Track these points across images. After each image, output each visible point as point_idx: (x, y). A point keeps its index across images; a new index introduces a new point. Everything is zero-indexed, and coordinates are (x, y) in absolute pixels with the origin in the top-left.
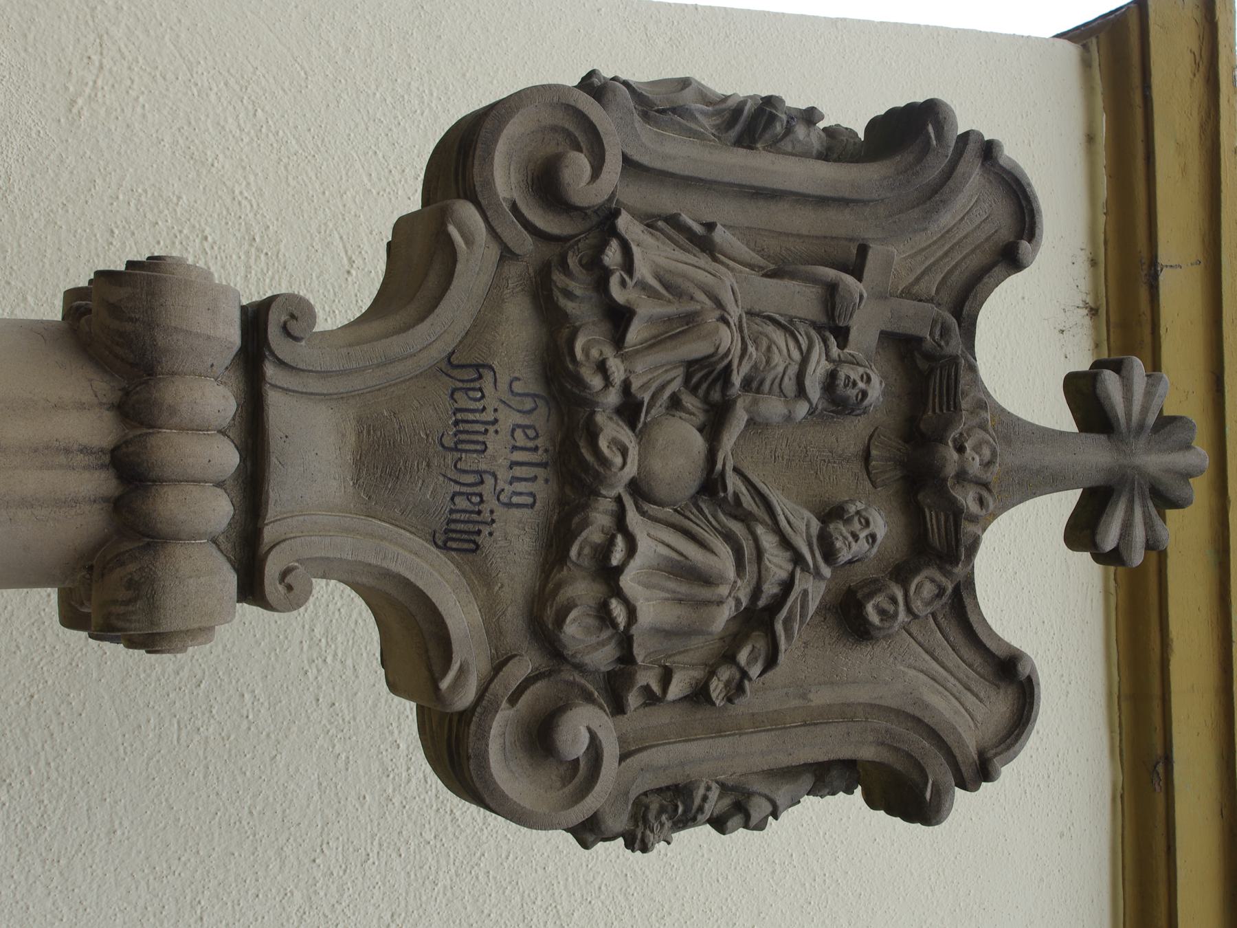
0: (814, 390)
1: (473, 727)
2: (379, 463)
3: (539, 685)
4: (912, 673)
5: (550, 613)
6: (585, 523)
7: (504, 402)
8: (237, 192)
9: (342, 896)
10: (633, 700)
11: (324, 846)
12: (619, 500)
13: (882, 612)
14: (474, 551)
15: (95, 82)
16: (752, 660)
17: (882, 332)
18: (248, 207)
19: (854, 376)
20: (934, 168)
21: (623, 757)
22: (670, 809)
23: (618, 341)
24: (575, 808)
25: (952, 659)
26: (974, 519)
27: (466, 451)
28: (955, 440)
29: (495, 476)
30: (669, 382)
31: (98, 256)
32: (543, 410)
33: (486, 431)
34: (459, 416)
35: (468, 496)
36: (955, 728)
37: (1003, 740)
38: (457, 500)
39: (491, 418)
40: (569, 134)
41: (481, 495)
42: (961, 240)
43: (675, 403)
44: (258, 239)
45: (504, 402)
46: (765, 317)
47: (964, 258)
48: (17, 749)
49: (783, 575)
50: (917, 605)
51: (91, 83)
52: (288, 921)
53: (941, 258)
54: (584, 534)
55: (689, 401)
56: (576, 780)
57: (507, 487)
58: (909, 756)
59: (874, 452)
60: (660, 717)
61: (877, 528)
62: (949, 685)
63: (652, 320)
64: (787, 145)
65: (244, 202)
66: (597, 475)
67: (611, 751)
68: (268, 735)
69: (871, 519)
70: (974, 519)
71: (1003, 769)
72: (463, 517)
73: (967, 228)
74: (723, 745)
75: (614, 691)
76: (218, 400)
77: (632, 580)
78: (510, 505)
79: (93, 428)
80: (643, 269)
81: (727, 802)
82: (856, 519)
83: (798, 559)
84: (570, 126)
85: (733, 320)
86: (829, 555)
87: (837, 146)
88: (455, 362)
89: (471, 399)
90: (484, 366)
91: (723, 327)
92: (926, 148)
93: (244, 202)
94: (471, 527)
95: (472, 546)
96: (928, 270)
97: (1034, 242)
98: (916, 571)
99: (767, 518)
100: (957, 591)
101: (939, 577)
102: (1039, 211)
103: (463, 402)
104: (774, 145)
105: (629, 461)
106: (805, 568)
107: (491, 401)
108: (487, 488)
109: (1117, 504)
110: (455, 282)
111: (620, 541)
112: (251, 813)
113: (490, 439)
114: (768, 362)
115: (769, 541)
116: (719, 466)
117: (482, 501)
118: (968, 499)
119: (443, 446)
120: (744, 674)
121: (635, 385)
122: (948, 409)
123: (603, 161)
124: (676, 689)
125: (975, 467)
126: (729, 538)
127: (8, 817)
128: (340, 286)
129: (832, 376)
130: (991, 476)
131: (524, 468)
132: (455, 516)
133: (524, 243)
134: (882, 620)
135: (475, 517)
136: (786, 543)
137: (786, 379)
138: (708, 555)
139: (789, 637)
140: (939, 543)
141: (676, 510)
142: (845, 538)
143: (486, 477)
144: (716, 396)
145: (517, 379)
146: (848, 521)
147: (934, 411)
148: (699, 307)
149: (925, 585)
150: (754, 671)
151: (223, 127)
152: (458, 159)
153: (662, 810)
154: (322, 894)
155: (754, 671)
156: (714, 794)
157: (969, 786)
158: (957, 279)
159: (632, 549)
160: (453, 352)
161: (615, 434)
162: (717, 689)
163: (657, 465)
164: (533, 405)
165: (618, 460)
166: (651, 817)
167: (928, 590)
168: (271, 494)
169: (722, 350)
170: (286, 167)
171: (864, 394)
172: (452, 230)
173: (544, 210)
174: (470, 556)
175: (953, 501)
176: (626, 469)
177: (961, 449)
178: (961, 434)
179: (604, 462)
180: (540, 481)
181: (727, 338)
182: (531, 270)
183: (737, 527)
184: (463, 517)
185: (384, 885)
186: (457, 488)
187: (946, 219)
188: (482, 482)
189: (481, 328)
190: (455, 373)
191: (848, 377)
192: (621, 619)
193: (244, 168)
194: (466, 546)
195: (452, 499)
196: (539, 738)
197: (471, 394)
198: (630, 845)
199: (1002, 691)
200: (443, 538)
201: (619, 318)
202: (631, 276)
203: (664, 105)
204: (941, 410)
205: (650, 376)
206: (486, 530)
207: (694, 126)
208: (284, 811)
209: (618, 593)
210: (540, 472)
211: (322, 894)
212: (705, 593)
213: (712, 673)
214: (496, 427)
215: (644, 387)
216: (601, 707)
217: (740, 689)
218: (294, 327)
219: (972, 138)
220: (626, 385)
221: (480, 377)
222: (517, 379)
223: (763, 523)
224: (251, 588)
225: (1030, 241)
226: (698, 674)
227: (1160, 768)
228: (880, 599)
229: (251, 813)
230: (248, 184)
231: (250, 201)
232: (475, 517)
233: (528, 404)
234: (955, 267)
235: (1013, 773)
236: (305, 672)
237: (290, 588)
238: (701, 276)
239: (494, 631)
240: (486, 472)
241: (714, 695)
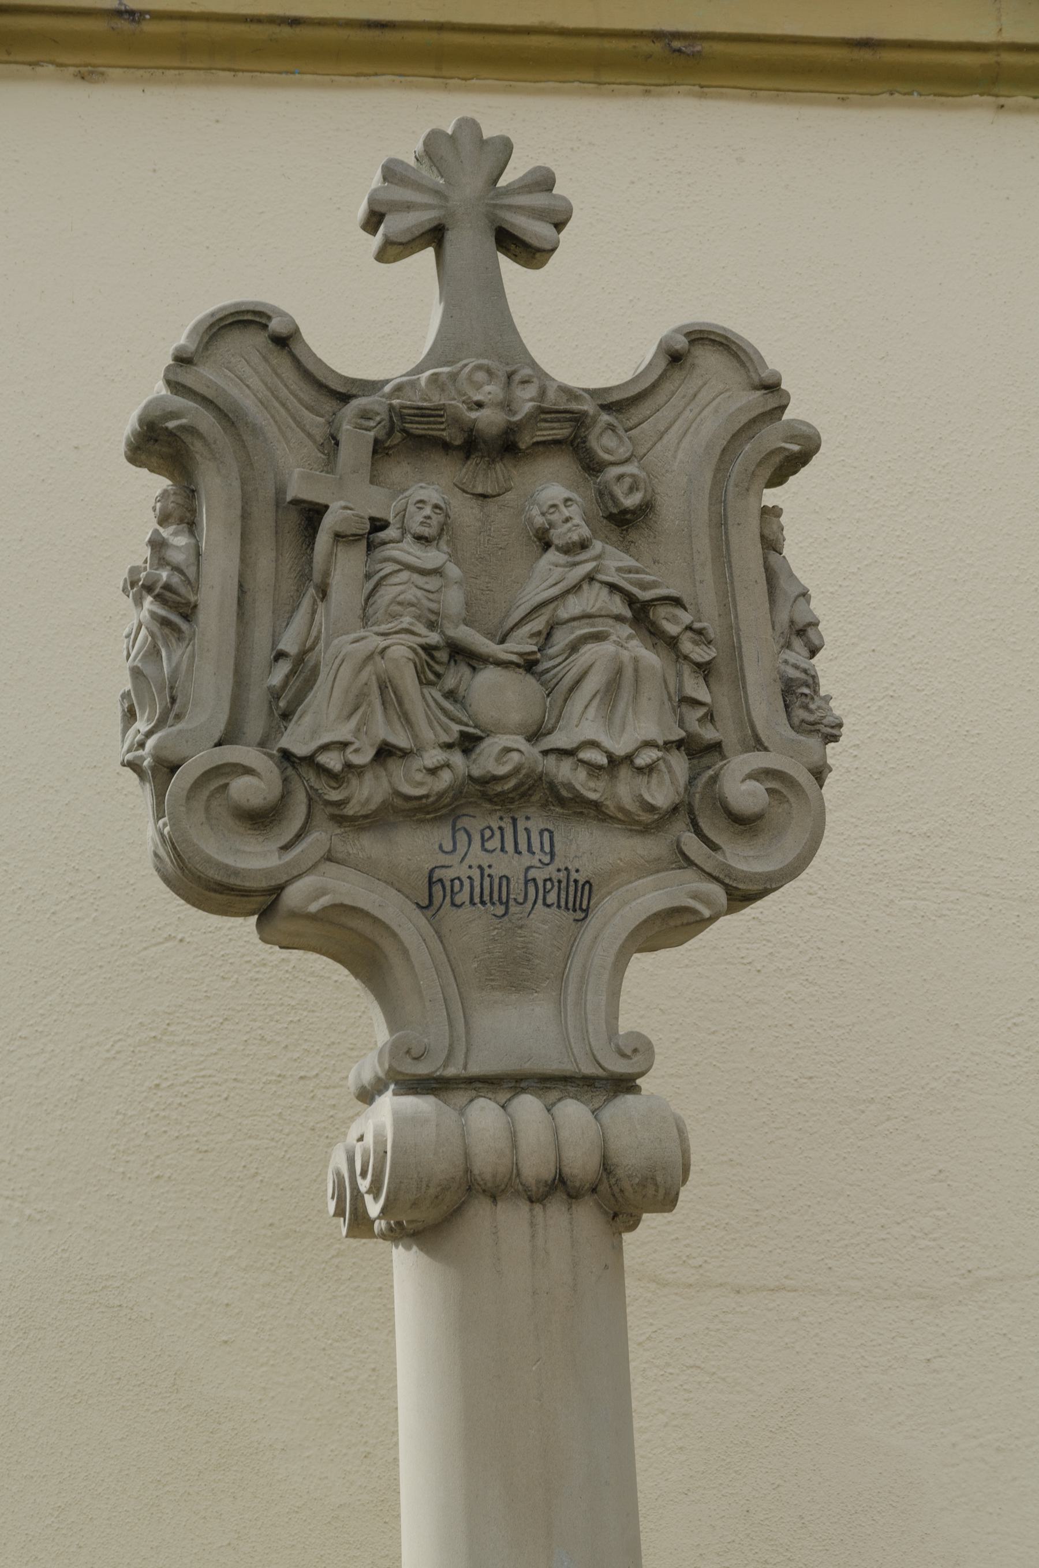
0: (432, 557)
1: (741, 886)
2: (514, 973)
3: (703, 823)
4: (680, 455)
5: (646, 817)
6: (569, 787)
7: (463, 859)
8: (108, 1055)
9: (791, 944)
10: (709, 734)
11: (745, 961)
12: (545, 753)
13: (632, 489)
14: (591, 885)
15: (7, 1198)
16: (674, 620)
17: (372, 482)
18: (120, 1043)
19: (419, 518)
20: (206, 421)
21: (759, 745)
22: (803, 699)
24: (808, 792)
25: (667, 413)
26: (543, 392)
27: (508, 894)
28: (470, 409)
29: (528, 869)
30: (435, 700)
31: (183, 1190)
33: (489, 876)
34: (477, 900)
35: (546, 893)
36: (731, 415)
37: (743, 364)
38: (549, 901)
39: (478, 871)
40: (212, 795)
41: (545, 881)
42: (269, 389)
43: (451, 695)
44: (153, 1034)
45: (463, 859)
46: (366, 604)
47: (286, 385)
48: (655, 1251)
49: (605, 591)
50: (623, 452)
51: (8, 1202)
52: (813, 996)
53: (288, 410)
54: (578, 787)
56: (783, 790)
57: (537, 857)
58: (759, 464)
59: (480, 490)
60: (725, 708)
61: (552, 490)
62: (691, 416)
63: (388, 721)
64: (191, 572)
65: (117, 1047)
66: (528, 776)
67: (758, 760)
68: (642, 1017)
69: (550, 503)
70: (543, 392)
71: (770, 367)
72: (563, 895)
73: (255, 381)
75: (700, 751)
76: (484, 1114)
77: (619, 743)
78: (552, 854)
79: (512, 1219)
80: (343, 732)
82: (549, 517)
83: (590, 578)
84: (206, 793)
85: (382, 642)
86: (584, 545)
88: (427, 902)
89: (461, 889)
90: (430, 877)
91: (389, 653)
92: (190, 430)
93: (117, 1047)
94: (572, 889)
95: (587, 887)
96: (298, 424)
97: (270, 313)
99: (552, 606)
100: (607, 408)
101: (597, 430)
102: (236, 305)
103: (463, 897)
104: (194, 585)
105: (515, 746)
106: (596, 570)
107: (463, 872)
108: (539, 875)
109: (512, 224)
110: (360, 905)
111: (587, 755)
112: (714, 1033)
113: (496, 872)
114: (412, 605)
115: (574, 606)
116: (514, 658)
117: (550, 879)
118: (526, 400)
119: (503, 915)
120: (689, 628)
121: (446, 739)
122: (441, 416)
123: (237, 764)
124: (702, 694)
125: (491, 391)
126: (574, 648)
127: (717, 1257)
128: (196, 949)
130: (501, 371)
131: (519, 841)
132: (563, 904)
133: (319, 838)
134: (637, 489)
135: (563, 885)
136: (576, 588)
137: (427, 587)
138: (593, 670)
139: (653, 585)
140: (569, 429)
141: (548, 695)
142: (569, 530)
143: (530, 877)
144: (443, 656)
145: (441, 847)
146: (552, 525)
147: (443, 430)
148: (374, 678)
149: (604, 443)
150: (686, 618)
151: (41, 1070)
152: (207, 888)
153: (806, 707)
154: (789, 963)
155: (686, 618)
156: (790, 656)
157: (785, 402)
158: (307, 393)
159: (594, 744)
160: (417, 904)
161: (492, 760)
162: (701, 654)
163: (515, 717)
164: (462, 831)
165: (515, 756)
166: (812, 718)
167: (609, 441)
168: (554, 1067)
169: (411, 655)
170: (78, 1006)
171: (436, 506)
172: (313, 908)
173: (265, 813)
174: (595, 888)
176: (522, 749)
177: (480, 405)
178: (463, 402)
179: (517, 770)
180: (529, 824)
181: (401, 650)
182: (338, 831)
183: (562, 639)
184: (563, 895)
185: (781, 902)
186: (540, 901)
187: (248, 402)
188: (534, 880)
189: (394, 882)
190: (437, 902)
191: (422, 523)
192: (653, 754)
193: (82, 1048)
194: (586, 892)
195: (549, 906)
196: (744, 823)
197: (457, 888)
199: (696, 361)
200: (579, 912)
201: (385, 753)
202: (352, 743)
203: (157, 694)
204: (442, 423)
205: (436, 724)
206: (574, 875)
207: (184, 666)
208: (713, 1001)
209: (629, 758)
210: (521, 824)
211: (789, 963)
213: (686, 658)
214: (485, 866)
215: (447, 730)
216: (721, 768)
217: (700, 632)
218: (415, 1052)
219: (172, 377)
221: (440, 880)
222: (441, 847)
223: (555, 610)
225: (269, 318)
227: (676, 44)
228: (619, 491)
229: (714, 1033)
230: (98, 1044)
231: (115, 1042)
232: (563, 885)
233: (462, 837)
234: (296, 396)
235: (776, 357)
237: (635, 1051)
239: (655, 867)
240: (526, 877)
241: (707, 658)
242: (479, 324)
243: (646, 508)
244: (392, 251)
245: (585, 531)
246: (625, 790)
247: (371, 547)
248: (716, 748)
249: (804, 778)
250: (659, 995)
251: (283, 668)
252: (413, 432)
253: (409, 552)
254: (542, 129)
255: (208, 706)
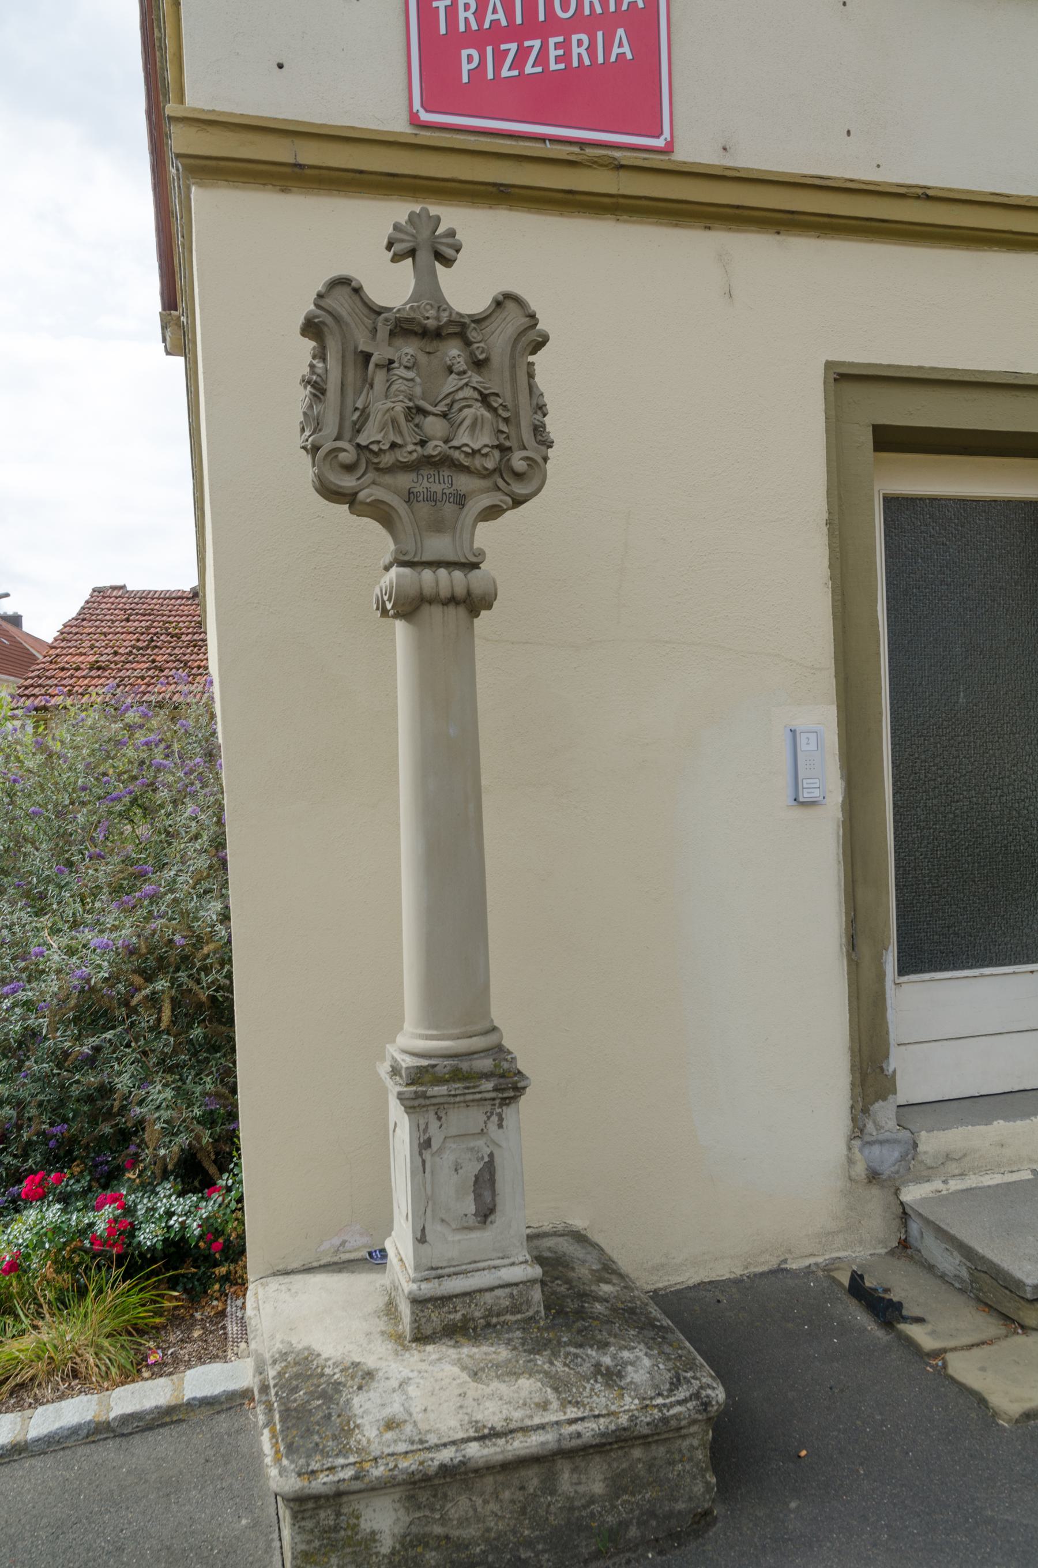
0: (410, 375)
2: (438, 526)
3: (505, 475)
5: (485, 472)
6: (458, 460)
10: (507, 444)
13: (482, 352)
16: (496, 401)
20: (329, 320)
21: (525, 448)
23: (400, 446)
25: (495, 325)
32: (421, 472)
43: (417, 426)
50: (479, 338)
55: (417, 421)
60: (513, 434)
63: (395, 434)
64: (324, 377)
67: (524, 454)
73: (346, 305)
74: (522, 413)
75: (504, 450)
76: (427, 574)
79: (436, 611)
80: (379, 437)
81: (539, 412)
83: (467, 384)
85: (393, 405)
86: (464, 372)
87: (321, 354)
96: (363, 323)
98: (467, 337)
100: (474, 321)
103: (421, 498)
104: (325, 382)
108: (447, 491)
113: (432, 490)
115: (460, 395)
118: (445, 317)
124: (505, 429)
125: (432, 313)
126: (461, 410)
129: (406, 367)
130: (436, 306)
136: (461, 388)
140: (460, 329)
144: (414, 411)
149: (473, 335)
150: (500, 401)
152: (330, 493)
156: (535, 416)
158: (366, 311)
159: (467, 445)
162: (505, 415)
163: (439, 435)
167: (474, 334)
172: (368, 500)
175: (446, 323)
177: (428, 318)
179: (440, 453)
181: (399, 408)
183: (456, 407)
187: (344, 314)
189: (396, 492)
196: (519, 476)
198: (551, 447)
201: (394, 446)
203: (313, 422)
209: (479, 451)
212: (480, 420)
217: (505, 406)
220: (415, 444)
224: (475, 566)
226: (500, 420)
228: (477, 353)
233: (420, 477)
235: (534, 306)
236: (501, 543)
238: (379, 416)
239: (488, 490)
242: (428, 289)
243: (487, 360)
244: (396, 258)
245: (465, 367)
246: (477, 462)
247: (389, 370)
248: (510, 449)
249: (540, 460)
250: (486, 536)
251: (357, 414)
252: (404, 327)
253: (402, 372)
254: (452, 217)
255: (330, 428)
